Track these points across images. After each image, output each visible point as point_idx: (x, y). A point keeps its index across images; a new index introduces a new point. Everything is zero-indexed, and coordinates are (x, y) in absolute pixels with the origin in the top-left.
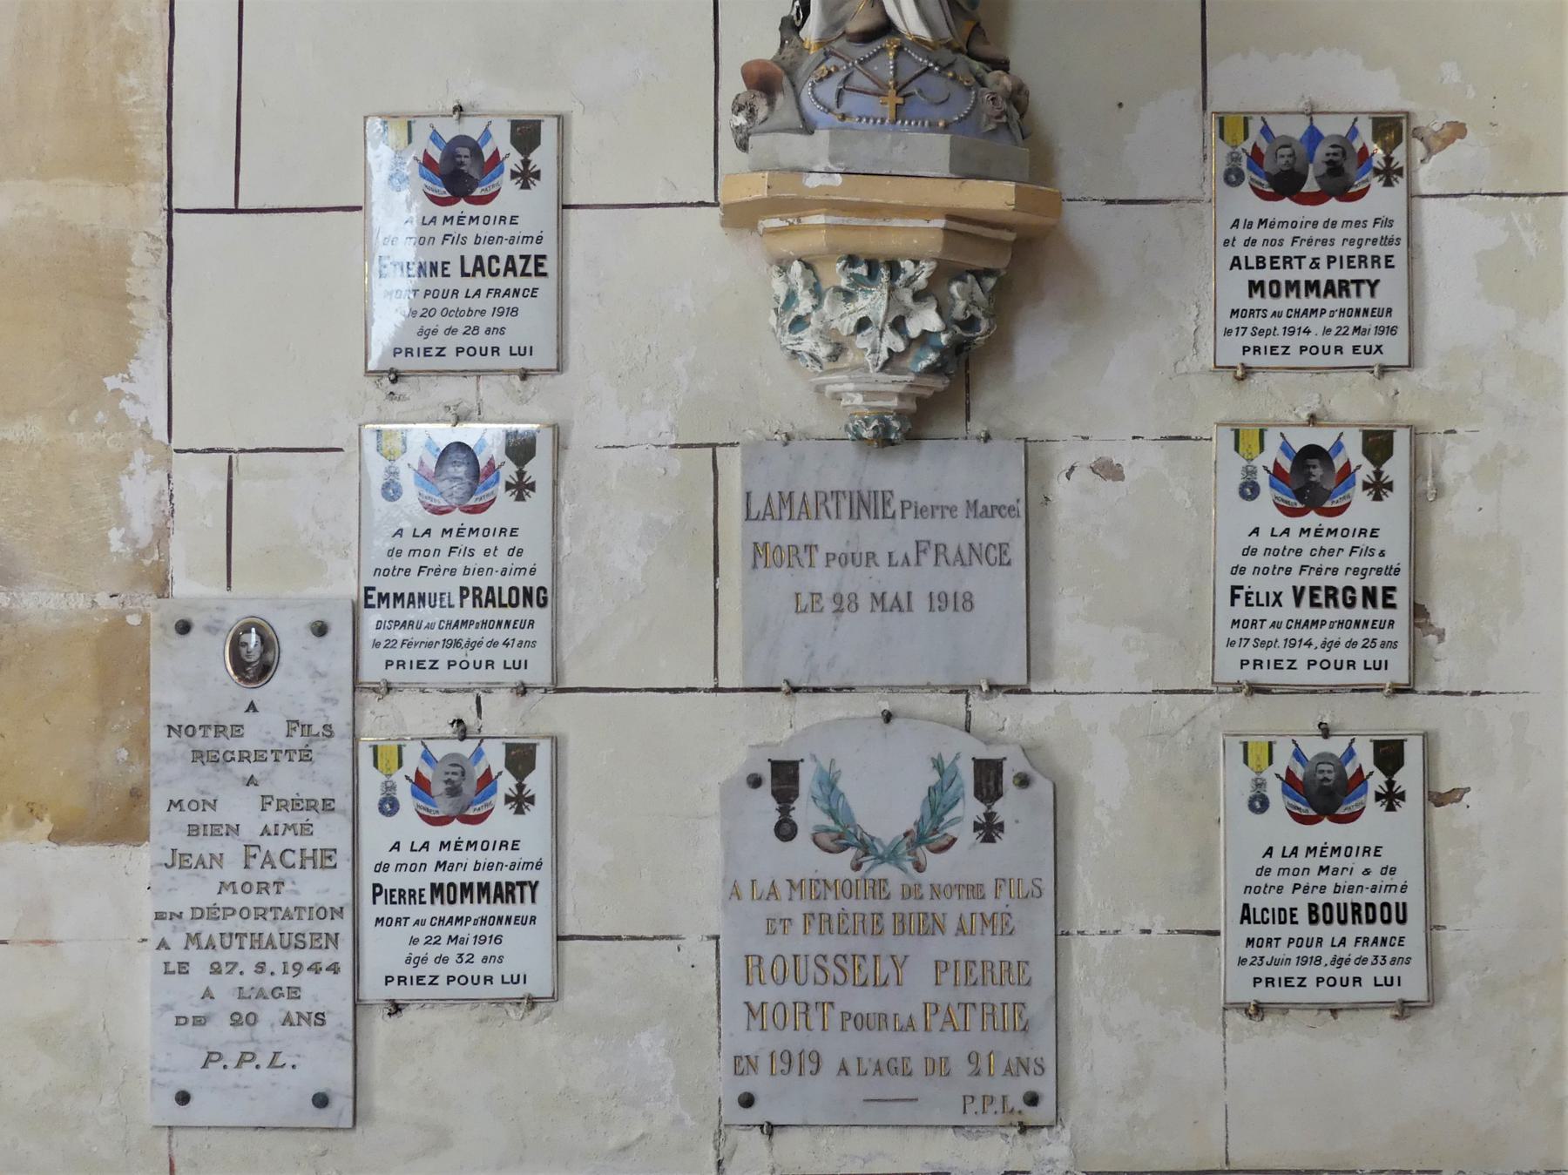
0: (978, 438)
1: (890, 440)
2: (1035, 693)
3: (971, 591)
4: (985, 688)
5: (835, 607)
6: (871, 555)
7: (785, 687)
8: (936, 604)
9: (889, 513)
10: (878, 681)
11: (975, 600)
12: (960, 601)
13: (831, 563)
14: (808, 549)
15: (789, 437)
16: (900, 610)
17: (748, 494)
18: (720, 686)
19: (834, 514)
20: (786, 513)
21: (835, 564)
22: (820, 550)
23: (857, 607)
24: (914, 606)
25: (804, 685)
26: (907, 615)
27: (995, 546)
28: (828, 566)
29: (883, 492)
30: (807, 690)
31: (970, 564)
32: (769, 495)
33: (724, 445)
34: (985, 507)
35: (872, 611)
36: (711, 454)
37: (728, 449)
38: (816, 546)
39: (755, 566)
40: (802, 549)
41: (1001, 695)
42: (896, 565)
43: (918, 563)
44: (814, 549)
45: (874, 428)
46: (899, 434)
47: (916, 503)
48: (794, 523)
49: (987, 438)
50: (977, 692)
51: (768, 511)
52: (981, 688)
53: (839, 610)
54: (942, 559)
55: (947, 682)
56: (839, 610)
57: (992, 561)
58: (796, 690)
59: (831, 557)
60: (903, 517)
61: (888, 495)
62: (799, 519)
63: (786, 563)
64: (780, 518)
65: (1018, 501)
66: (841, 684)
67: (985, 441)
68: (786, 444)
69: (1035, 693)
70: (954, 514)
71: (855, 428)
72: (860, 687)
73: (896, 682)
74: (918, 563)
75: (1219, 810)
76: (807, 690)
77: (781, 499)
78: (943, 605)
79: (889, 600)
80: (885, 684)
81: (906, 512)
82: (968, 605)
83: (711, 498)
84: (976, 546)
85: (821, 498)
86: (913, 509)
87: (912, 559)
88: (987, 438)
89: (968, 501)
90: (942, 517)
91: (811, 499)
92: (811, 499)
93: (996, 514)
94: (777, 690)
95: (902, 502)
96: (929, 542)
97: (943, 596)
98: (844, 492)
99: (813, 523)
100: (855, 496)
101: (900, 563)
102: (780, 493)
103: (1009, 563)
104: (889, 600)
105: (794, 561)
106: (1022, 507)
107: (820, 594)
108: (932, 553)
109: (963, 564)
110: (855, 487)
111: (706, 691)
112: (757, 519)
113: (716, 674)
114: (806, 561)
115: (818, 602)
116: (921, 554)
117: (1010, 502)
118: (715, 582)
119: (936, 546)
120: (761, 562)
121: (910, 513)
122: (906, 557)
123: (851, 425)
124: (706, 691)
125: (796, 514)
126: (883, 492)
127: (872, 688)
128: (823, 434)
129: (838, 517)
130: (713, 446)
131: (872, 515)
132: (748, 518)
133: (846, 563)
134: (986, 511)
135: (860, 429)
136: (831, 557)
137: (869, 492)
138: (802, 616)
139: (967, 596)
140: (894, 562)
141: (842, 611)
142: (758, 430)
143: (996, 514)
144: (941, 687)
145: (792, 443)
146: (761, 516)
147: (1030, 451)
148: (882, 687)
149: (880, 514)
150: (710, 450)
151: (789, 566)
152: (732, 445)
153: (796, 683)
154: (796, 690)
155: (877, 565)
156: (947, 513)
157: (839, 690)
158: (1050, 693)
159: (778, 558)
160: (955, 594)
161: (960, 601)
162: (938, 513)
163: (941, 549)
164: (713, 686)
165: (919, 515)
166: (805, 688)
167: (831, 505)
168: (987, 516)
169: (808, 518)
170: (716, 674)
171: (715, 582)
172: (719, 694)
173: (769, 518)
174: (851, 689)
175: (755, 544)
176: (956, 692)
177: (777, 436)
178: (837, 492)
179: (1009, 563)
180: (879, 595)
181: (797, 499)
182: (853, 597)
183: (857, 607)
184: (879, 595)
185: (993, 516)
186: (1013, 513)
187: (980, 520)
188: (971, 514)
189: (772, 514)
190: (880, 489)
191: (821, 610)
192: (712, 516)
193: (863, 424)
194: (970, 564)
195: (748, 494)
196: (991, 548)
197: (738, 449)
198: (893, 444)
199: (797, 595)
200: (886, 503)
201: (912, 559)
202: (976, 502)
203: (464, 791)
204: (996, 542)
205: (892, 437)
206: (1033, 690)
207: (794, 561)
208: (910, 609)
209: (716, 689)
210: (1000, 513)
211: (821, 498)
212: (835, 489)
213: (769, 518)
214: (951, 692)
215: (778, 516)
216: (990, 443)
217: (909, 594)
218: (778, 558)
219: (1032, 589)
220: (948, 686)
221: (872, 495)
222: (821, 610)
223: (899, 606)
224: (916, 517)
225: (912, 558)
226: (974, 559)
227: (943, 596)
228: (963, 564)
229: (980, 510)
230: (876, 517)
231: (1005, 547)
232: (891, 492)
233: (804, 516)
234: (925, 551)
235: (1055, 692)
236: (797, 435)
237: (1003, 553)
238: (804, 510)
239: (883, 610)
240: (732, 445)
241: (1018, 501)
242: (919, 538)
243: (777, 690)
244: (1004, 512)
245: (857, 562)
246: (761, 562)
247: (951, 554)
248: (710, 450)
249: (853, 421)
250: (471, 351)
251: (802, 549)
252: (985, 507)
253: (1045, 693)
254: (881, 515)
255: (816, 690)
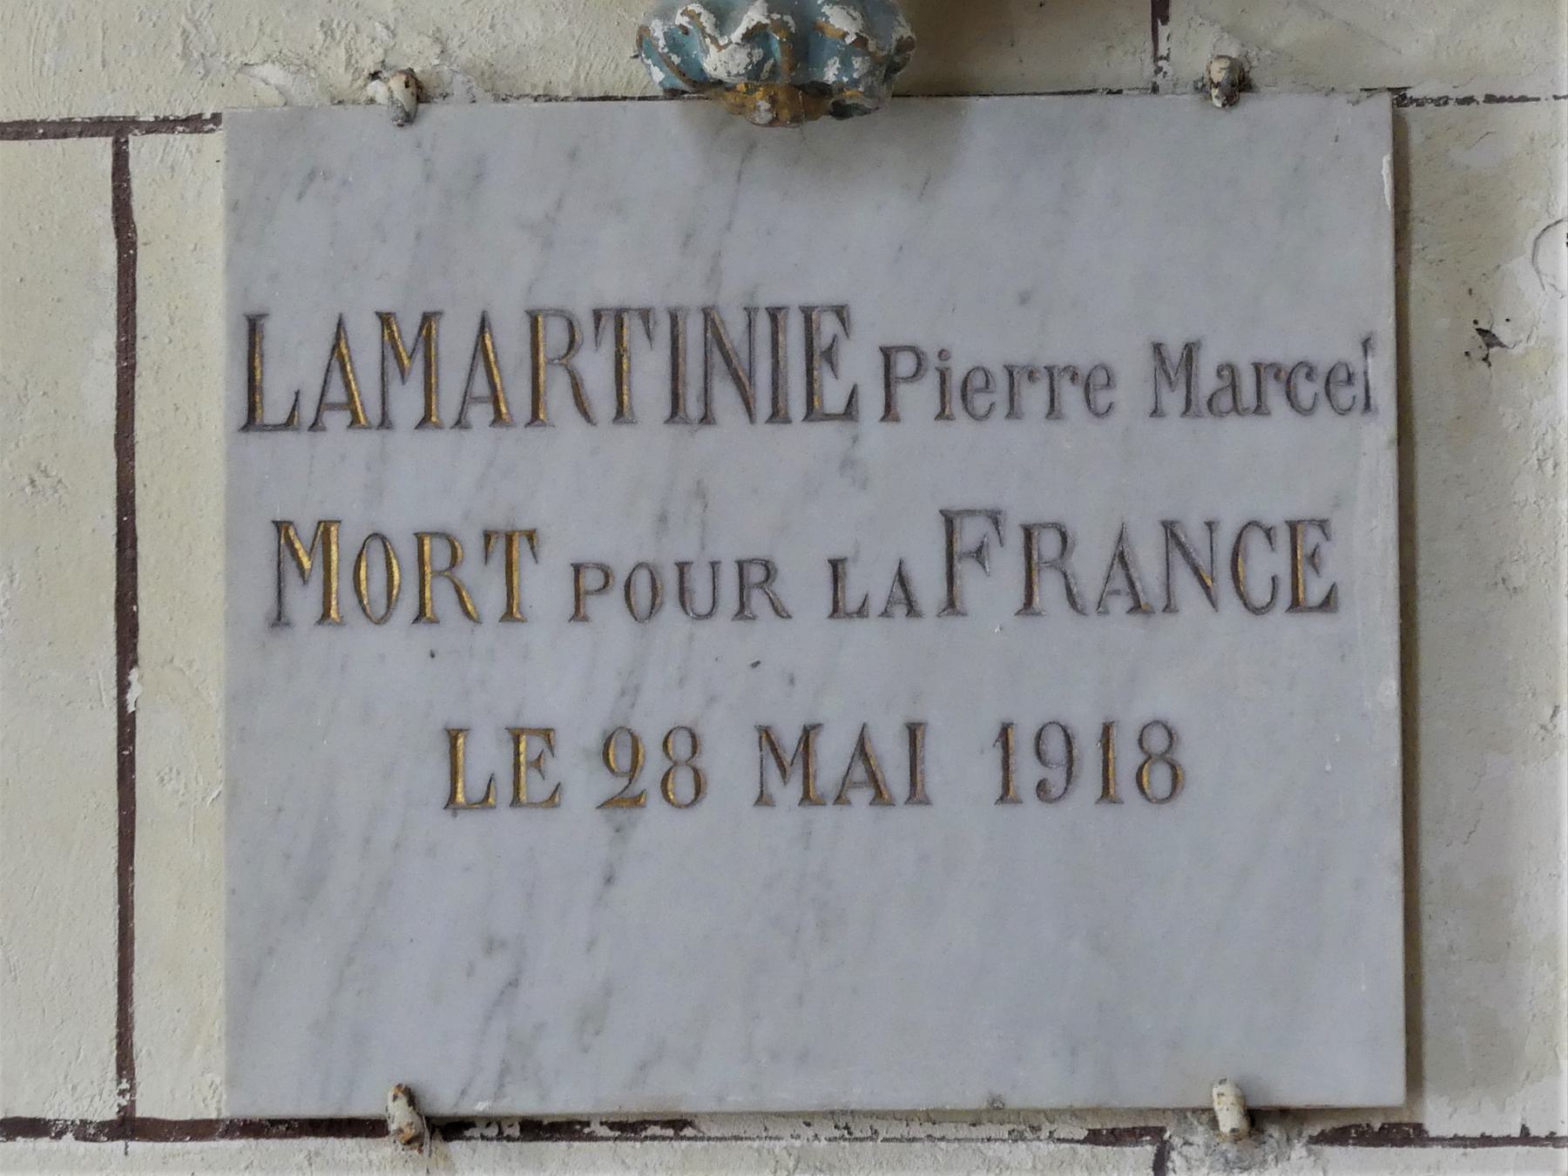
0: (1202, 88)
1: (823, 90)
2: (1440, 1140)
3: (1173, 719)
4: (1229, 1119)
5: (612, 786)
6: (756, 574)
7: (399, 1115)
8: (1027, 772)
9: (834, 397)
10: (788, 1093)
11: (1185, 756)
12: (1127, 758)
13: (593, 605)
14: (499, 547)
15: (420, 91)
16: (880, 796)
17: (254, 327)
18: (142, 1112)
19: (603, 404)
20: (407, 401)
21: (608, 609)
22: (544, 551)
23: (699, 789)
24: (934, 778)
25: (481, 1107)
26: (904, 817)
27: (1269, 533)
28: (578, 615)
29: (807, 313)
30: (498, 1128)
31: (1169, 608)
32: (340, 325)
33: (164, 125)
34: (1228, 371)
35: (763, 800)
36: (107, 163)
37: (181, 141)
38: (531, 536)
39: (279, 620)
40: (471, 546)
41: (1299, 1151)
42: (861, 612)
43: (951, 605)
44: (521, 548)
45: (755, 36)
46: (857, 63)
47: (943, 354)
48: (440, 442)
49: (1239, 86)
50: (1200, 1136)
51: (336, 394)
52: (1214, 1123)
53: (626, 801)
54: (1049, 589)
55: (1080, 1097)
56: (626, 801)
57: (1260, 594)
58: (452, 1128)
59: (592, 579)
60: (890, 412)
61: (828, 326)
62: (461, 423)
63: (407, 606)
64: (385, 423)
65: (1366, 345)
66: (633, 1105)
67: (1230, 100)
68: (408, 119)
69: (1440, 1140)
70: (1102, 399)
71: (677, 41)
72: (712, 1116)
73: (858, 1096)
74: (951, 605)
75: (1381, 168)
76: (498, 1128)
77: (390, 342)
78: (1056, 777)
79: (832, 756)
80: (811, 1103)
81: (904, 392)
82: (1159, 779)
83: (107, 340)
84: (1194, 535)
85: (554, 336)
86: (931, 381)
87: (930, 588)
88: (1239, 86)
89: (1157, 348)
90: (1053, 411)
91: (511, 344)
92: (511, 344)
93: (1275, 395)
94: (372, 1128)
95: (887, 354)
96: (995, 518)
97: (1055, 746)
98: (645, 315)
99: (518, 441)
100: (693, 331)
101: (877, 604)
102: (385, 319)
103: (1328, 603)
104: (832, 756)
105: (442, 597)
106: (1381, 371)
107: (547, 734)
108: (1008, 561)
109: (1137, 608)
110: (692, 296)
111: (85, 1131)
112: (289, 424)
113: (125, 1064)
114: (491, 598)
115: (537, 764)
116: (966, 569)
117: (1333, 348)
118: (123, 686)
119: (1028, 533)
120: (304, 602)
121: (918, 398)
122: (902, 579)
123: (658, 30)
124: (85, 1131)
125: (448, 405)
126: (807, 313)
127: (767, 1121)
128: (563, 78)
129: (621, 414)
130: (118, 130)
131: (763, 406)
132: (252, 421)
133: (654, 607)
134: (1234, 387)
135: (694, 45)
136: (592, 579)
137: (750, 312)
138: (470, 823)
139: (1157, 741)
140: (852, 600)
141: (636, 801)
142: (302, 66)
143: (1275, 395)
144: (1052, 1115)
145: (435, 113)
146: (307, 412)
147: (1416, 138)
148: (808, 1119)
149: (796, 404)
150: (102, 148)
151: (420, 615)
152: (194, 123)
153: (446, 1104)
154: (452, 1128)
155: (780, 611)
156: (1071, 396)
157: (628, 1128)
158: (1508, 1141)
159: (374, 586)
160: (1107, 729)
161: (1127, 758)
162: (1034, 397)
163: (1048, 545)
164: (111, 1114)
165: (956, 405)
166: (489, 1121)
167: (595, 366)
168: (1236, 408)
169: (498, 419)
170: (125, 1064)
171: (123, 686)
172: (136, 1146)
173: (336, 421)
174: (678, 1125)
175: (281, 527)
176: (1116, 1137)
177: (377, 89)
178: (619, 316)
179: (1328, 603)
180: (789, 740)
181: (455, 343)
182: (681, 747)
183: (699, 789)
184: (789, 740)
185: (1260, 409)
186: (1344, 396)
187: (1207, 424)
188: (1173, 401)
189: (350, 404)
190: (792, 297)
191: (552, 801)
192: (112, 415)
193: (707, 20)
194: (1169, 608)
195: (254, 327)
196: (1256, 541)
197: (213, 143)
198: (841, 111)
199: (453, 736)
200: (819, 357)
201: (930, 588)
202: (1190, 351)
203: (1120, 588)
204: (1276, 516)
205: (830, 74)
206: (1436, 1125)
207: (442, 597)
208: (917, 794)
209: (127, 1127)
210: (1291, 397)
211: (554, 336)
212: (612, 300)
213: (336, 421)
214: (1094, 1138)
215: (374, 414)
216: (1249, 105)
217: (914, 732)
218: (374, 586)
219: (1430, 728)
220: (1076, 1114)
221: (763, 325)
222: (552, 801)
223: (874, 780)
224: (942, 415)
225: (929, 586)
226: (1185, 582)
227: (1055, 746)
228: (1137, 608)
229: (1207, 382)
230: (778, 415)
231: (1312, 537)
232: (841, 312)
233: (480, 414)
234: (979, 554)
235: (1526, 1138)
236: (458, 88)
237: (1303, 561)
238: (481, 387)
239: (807, 798)
240: (194, 123)
241: (1366, 345)
242: (957, 502)
243: (372, 1128)
244: (1307, 391)
245: (702, 602)
246: (304, 602)
247: (1090, 564)
248: (102, 148)
249: (665, 14)
251: (471, 546)
252: (1228, 371)
253: (1486, 1141)
254: (797, 406)
255: (535, 1129)
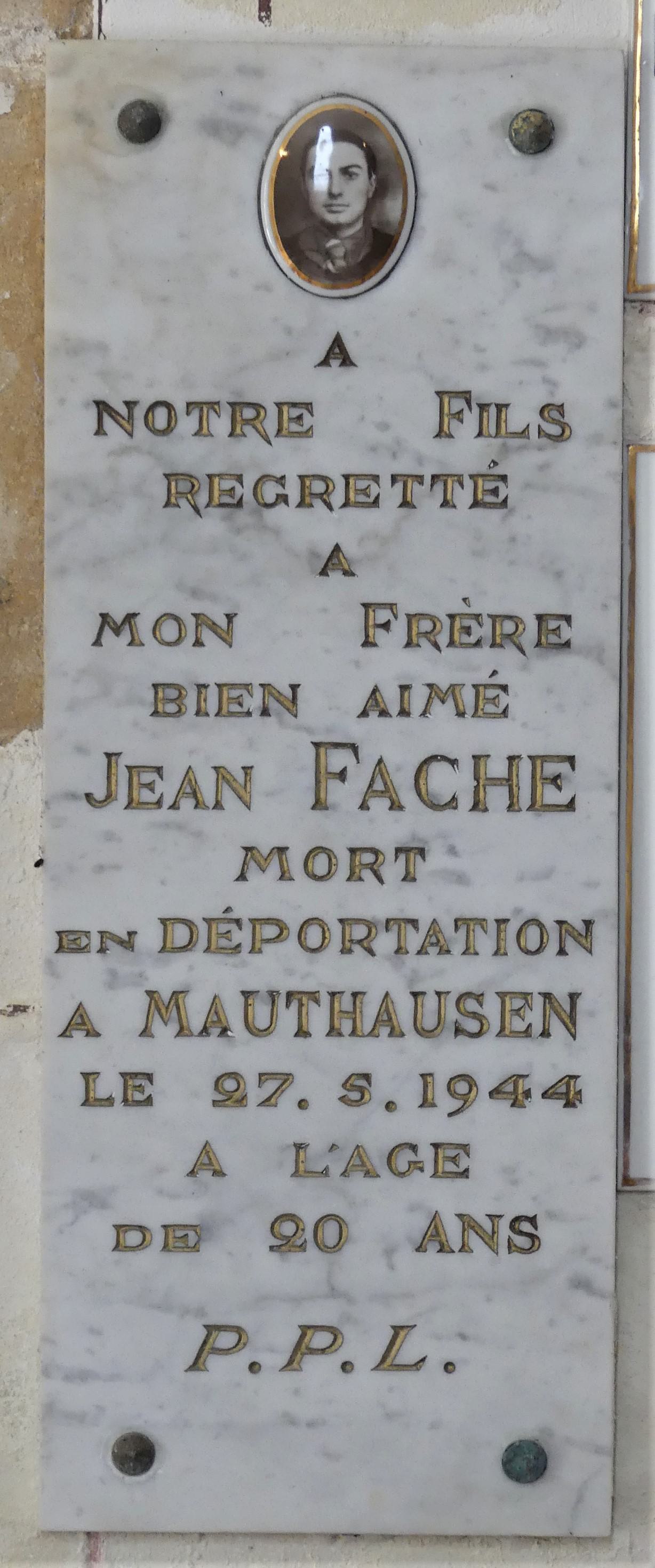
250: (314, 936)
